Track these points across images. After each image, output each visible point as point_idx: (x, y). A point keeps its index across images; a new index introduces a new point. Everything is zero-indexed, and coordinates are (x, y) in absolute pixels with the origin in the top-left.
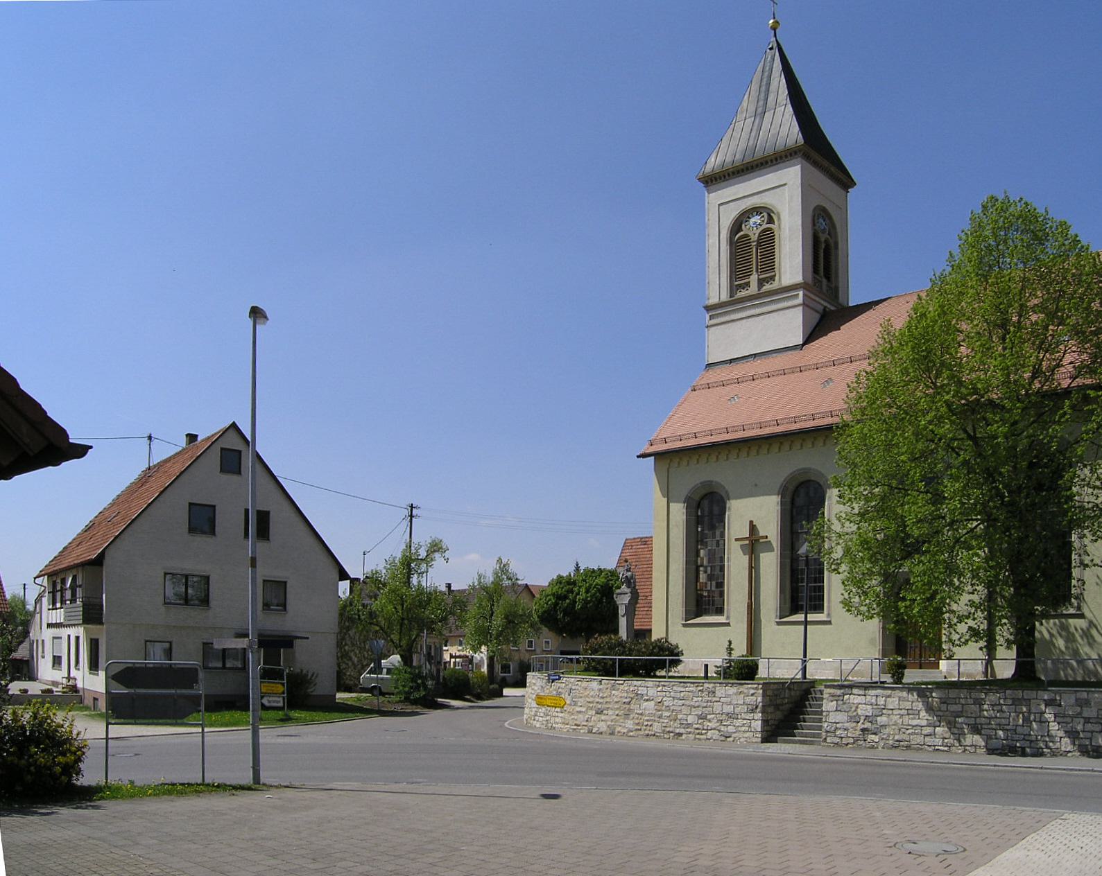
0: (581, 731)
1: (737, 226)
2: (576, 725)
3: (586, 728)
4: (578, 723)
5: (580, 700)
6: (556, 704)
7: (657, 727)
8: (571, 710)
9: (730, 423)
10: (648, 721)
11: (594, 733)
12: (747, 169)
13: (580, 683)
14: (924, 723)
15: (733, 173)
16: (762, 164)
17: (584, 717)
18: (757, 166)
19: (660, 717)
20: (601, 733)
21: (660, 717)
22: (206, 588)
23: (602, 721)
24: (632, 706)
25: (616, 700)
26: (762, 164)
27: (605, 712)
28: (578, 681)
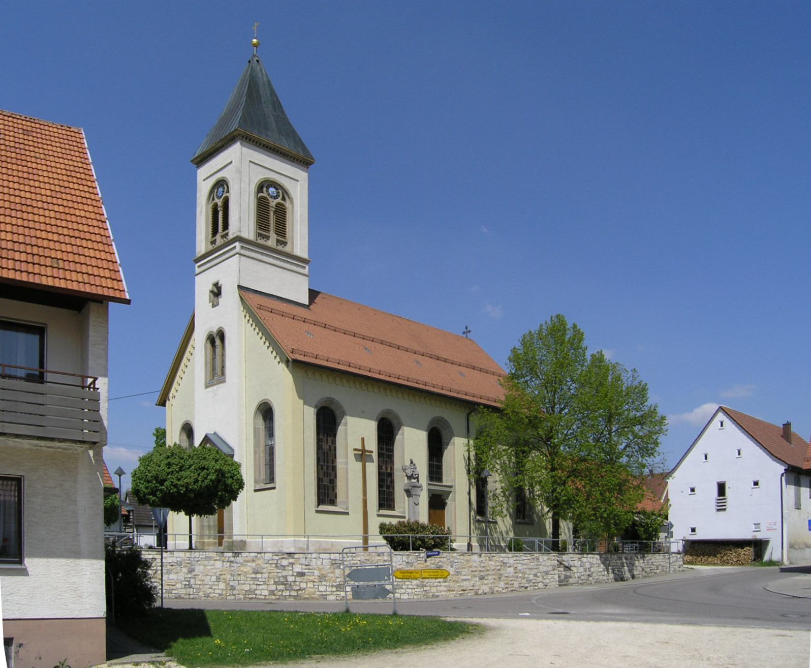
0: (469, 594)
1: (261, 187)
2: (463, 590)
3: (473, 591)
4: (464, 588)
5: (463, 570)
6: (438, 575)
7: (516, 584)
8: (456, 579)
9: (373, 366)
10: (511, 581)
11: (480, 594)
12: (274, 150)
13: (462, 557)
14: (602, 570)
15: (264, 145)
16: (284, 154)
17: (470, 583)
18: (281, 153)
19: (517, 577)
20: (485, 594)
21: (517, 577)
22: (13, 372)
23: (485, 584)
24: (502, 572)
25: (493, 568)
26: (284, 154)
27: (486, 577)
28: (461, 555)
